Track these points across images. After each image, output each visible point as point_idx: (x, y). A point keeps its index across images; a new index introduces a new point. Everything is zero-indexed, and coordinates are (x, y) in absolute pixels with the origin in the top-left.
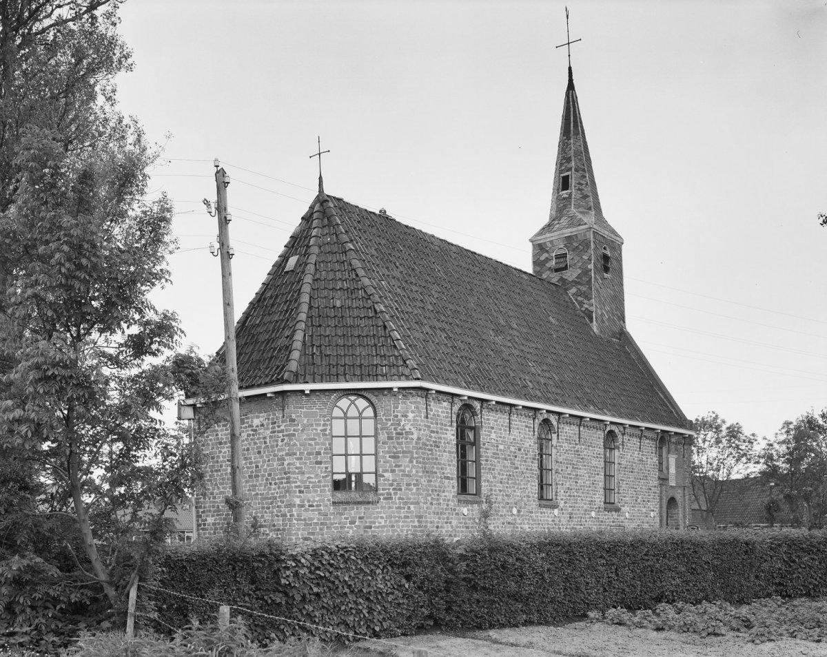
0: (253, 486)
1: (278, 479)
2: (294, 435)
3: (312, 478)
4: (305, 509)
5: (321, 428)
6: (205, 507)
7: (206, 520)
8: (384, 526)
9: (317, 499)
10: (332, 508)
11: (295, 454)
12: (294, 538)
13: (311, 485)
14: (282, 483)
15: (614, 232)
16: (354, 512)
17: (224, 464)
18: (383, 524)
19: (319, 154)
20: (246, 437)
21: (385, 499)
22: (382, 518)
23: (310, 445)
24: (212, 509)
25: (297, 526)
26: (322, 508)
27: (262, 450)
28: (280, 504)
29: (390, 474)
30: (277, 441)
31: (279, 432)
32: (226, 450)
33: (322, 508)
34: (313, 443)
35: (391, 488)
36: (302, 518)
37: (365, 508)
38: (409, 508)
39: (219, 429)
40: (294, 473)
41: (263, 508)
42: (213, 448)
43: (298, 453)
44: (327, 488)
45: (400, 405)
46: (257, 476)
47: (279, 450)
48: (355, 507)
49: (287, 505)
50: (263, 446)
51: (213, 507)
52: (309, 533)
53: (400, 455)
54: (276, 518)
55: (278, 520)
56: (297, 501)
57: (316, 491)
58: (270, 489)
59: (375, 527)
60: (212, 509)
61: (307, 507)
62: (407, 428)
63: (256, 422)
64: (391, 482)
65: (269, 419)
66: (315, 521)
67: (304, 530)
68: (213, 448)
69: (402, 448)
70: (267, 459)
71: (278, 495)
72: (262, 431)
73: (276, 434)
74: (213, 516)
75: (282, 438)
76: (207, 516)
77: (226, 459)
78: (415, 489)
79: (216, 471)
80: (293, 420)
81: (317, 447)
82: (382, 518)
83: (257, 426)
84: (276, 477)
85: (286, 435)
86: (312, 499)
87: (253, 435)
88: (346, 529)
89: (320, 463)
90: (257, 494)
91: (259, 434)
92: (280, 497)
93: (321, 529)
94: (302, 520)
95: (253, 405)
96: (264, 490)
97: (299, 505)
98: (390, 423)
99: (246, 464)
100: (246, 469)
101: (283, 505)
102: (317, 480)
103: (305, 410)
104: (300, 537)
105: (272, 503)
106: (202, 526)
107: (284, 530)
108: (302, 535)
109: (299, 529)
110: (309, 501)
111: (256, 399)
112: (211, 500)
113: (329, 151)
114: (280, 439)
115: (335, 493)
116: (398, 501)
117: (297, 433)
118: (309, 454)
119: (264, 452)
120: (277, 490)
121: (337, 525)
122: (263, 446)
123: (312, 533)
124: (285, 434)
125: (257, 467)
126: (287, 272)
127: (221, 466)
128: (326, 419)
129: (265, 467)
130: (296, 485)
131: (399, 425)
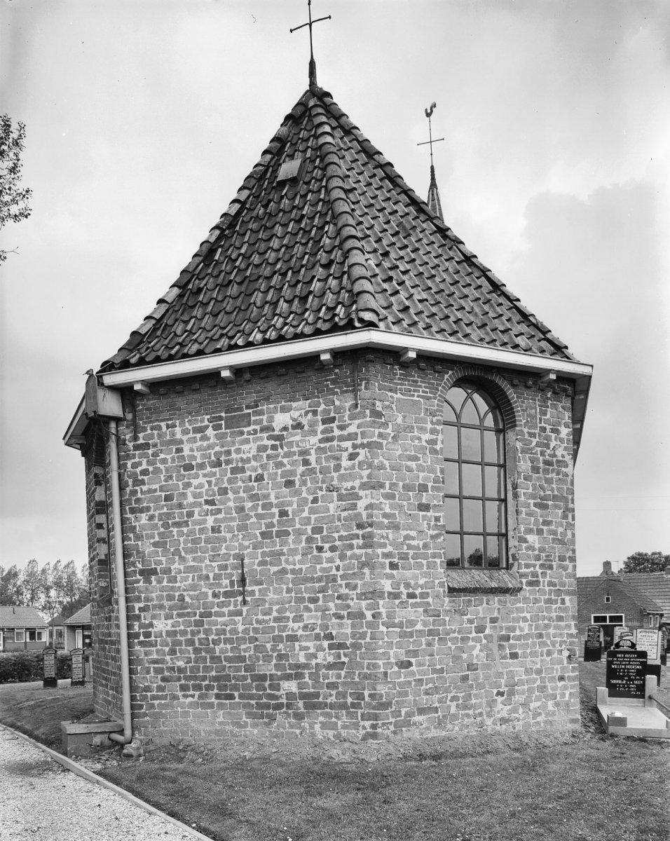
0: (272, 554)
1: (341, 538)
2: (380, 446)
3: (413, 538)
4: (402, 603)
5: (427, 436)
6: (147, 599)
7: (151, 625)
8: (527, 637)
9: (421, 582)
10: (447, 599)
11: (382, 486)
12: (380, 662)
13: (411, 552)
14: (351, 547)
16: (483, 609)
17: (197, 510)
18: (526, 631)
19: (310, 25)
20: (254, 452)
23: (409, 469)
24: (166, 603)
25: (386, 639)
26: (430, 600)
27: (297, 479)
28: (344, 591)
29: (536, 537)
30: (338, 459)
31: (341, 439)
32: (202, 480)
33: (430, 600)
34: (413, 464)
35: (538, 563)
36: (396, 621)
37: (500, 601)
38: (563, 601)
39: (185, 438)
40: (381, 526)
41: (301, 600)
42: (171, 477)
43: (387, 486)
44: (438, 561)
45: (549, 410)
46: (283, 534)
47: (342, 478)
48: (485, 598)
49: (362, 594)
50: (301, 469)
51: (170, 598)
52: (408, 653)
53: (550, 503)
54: (334, 620)
55: (341, 626)
56: (387, 586)
57: (420, 566)
58: (318, 560)
60: (166, 603)
61: (404, 597)
62: (559, 452)
63: (281, 420)
64: (536, 552)
65: (315, 413)
66: (419, 627)
67: (399, 646)
68: (171, 477)
69: (552, 490)
70: (311, 498)
71: (341, 572)
72: (298, 438)
73: (335, 443)
74: (168, 617)
75: (351, 450)
76: (154, 617)
77: (202, 500)
79: (177, 524)
80: (379, 415)
81: (421, 474)
83: (285, 429)
84: (336, 535)
85: (363, 446)
86: (412, 582)
87: (274, 447)
88: (471, 643)
89: (425, 508)
90: (284, 571)
91: (290, 444)
92: (343, 577)
93: (429, 644)
94: (394, 626)
95: (271, 386)
96: (301, 562)
97: (390, 593)
98: (534, 441)
99: (255, 508)
100: (254, 520)
101: (353, 593)
102: (421, 544)
103: (399, 395)
104: (392, 660)
105: (323, 590)
106: (142, 638)
107: (356, 646)
108: (396, 655)
109: (390, 645)
110: (407, 585)
111: (283, 371)
112: (165, 583)
113: (330, 17)
114: (345, 455)
115: (449, 572)
116: (547, 588)
117: (385, 442)
118: (407, 488)
119: (304, 483)
120: (338, 562)
121: (456, 635)
122: (301, 469)
123: (414, 651)
124: (359, 442)
125: (283, 513)
126: (282, 184)
127: (190, 514)
128: (435, 419)
129: (305, 514)
130: (385, 551)
131: (547, 446)
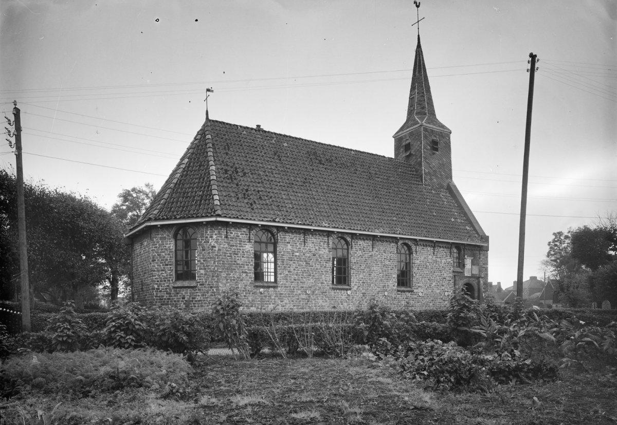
15: (443, 126)
21: (200, 285)
22: (199, 296)
59: (195, 301)
66: (165, 297)
67: (159, 302)
78: (216, 279)
82: (199, 296)
98: (203, 242)
131: (208, 242)
